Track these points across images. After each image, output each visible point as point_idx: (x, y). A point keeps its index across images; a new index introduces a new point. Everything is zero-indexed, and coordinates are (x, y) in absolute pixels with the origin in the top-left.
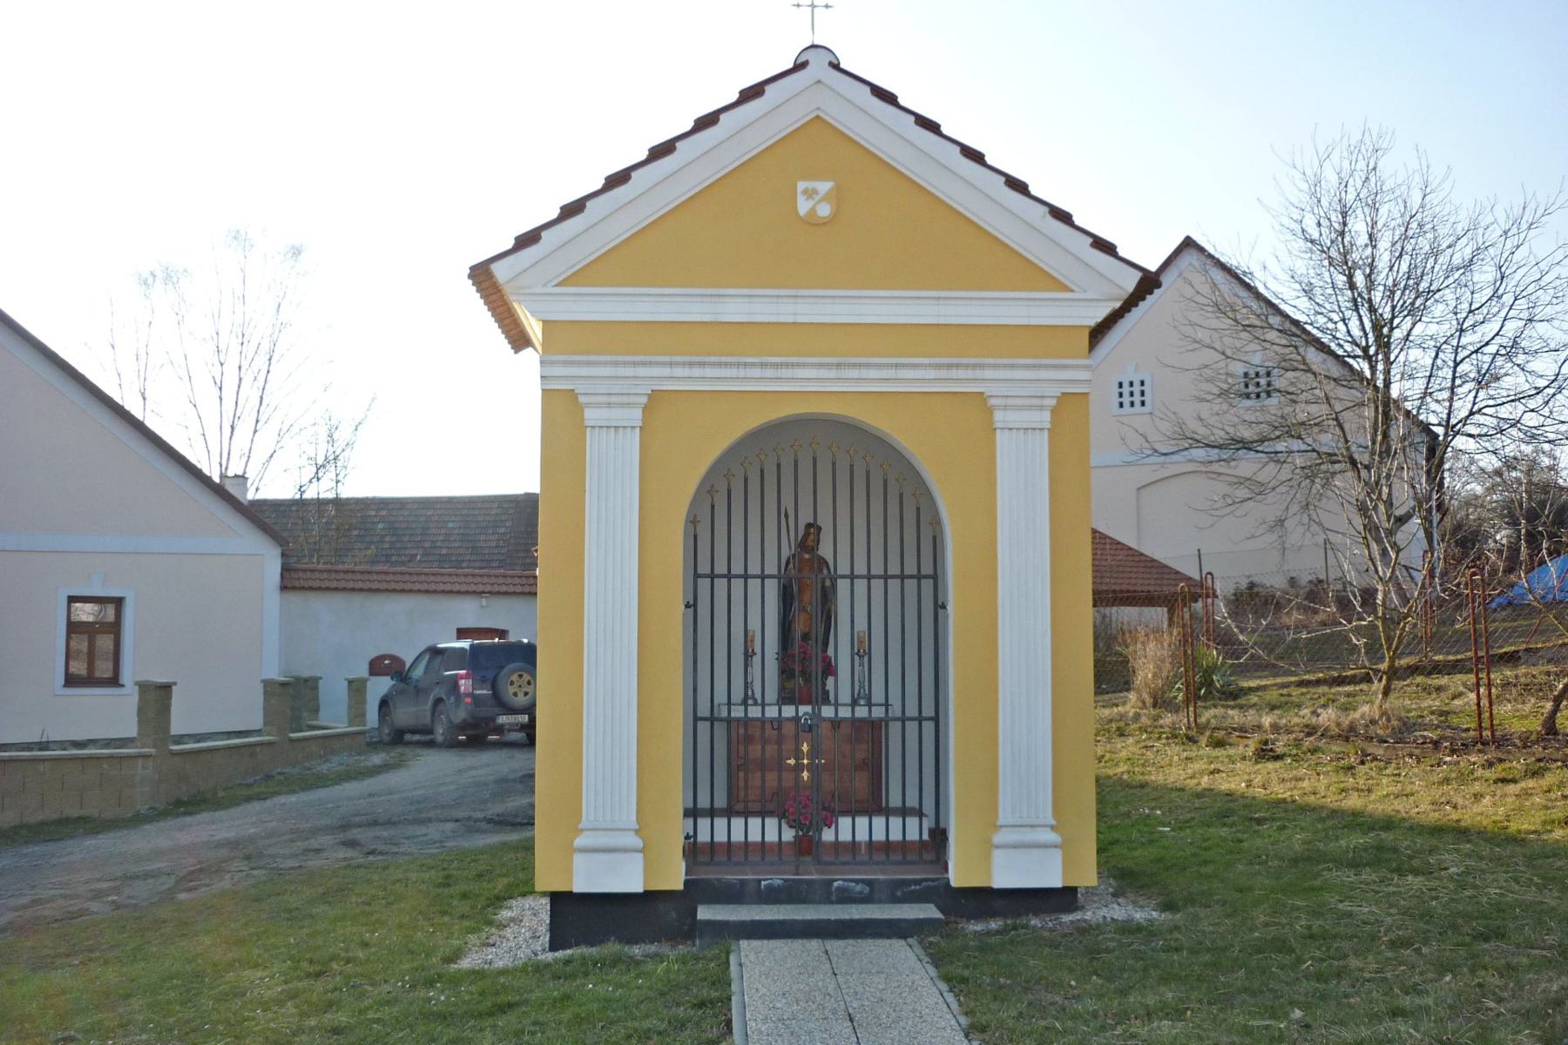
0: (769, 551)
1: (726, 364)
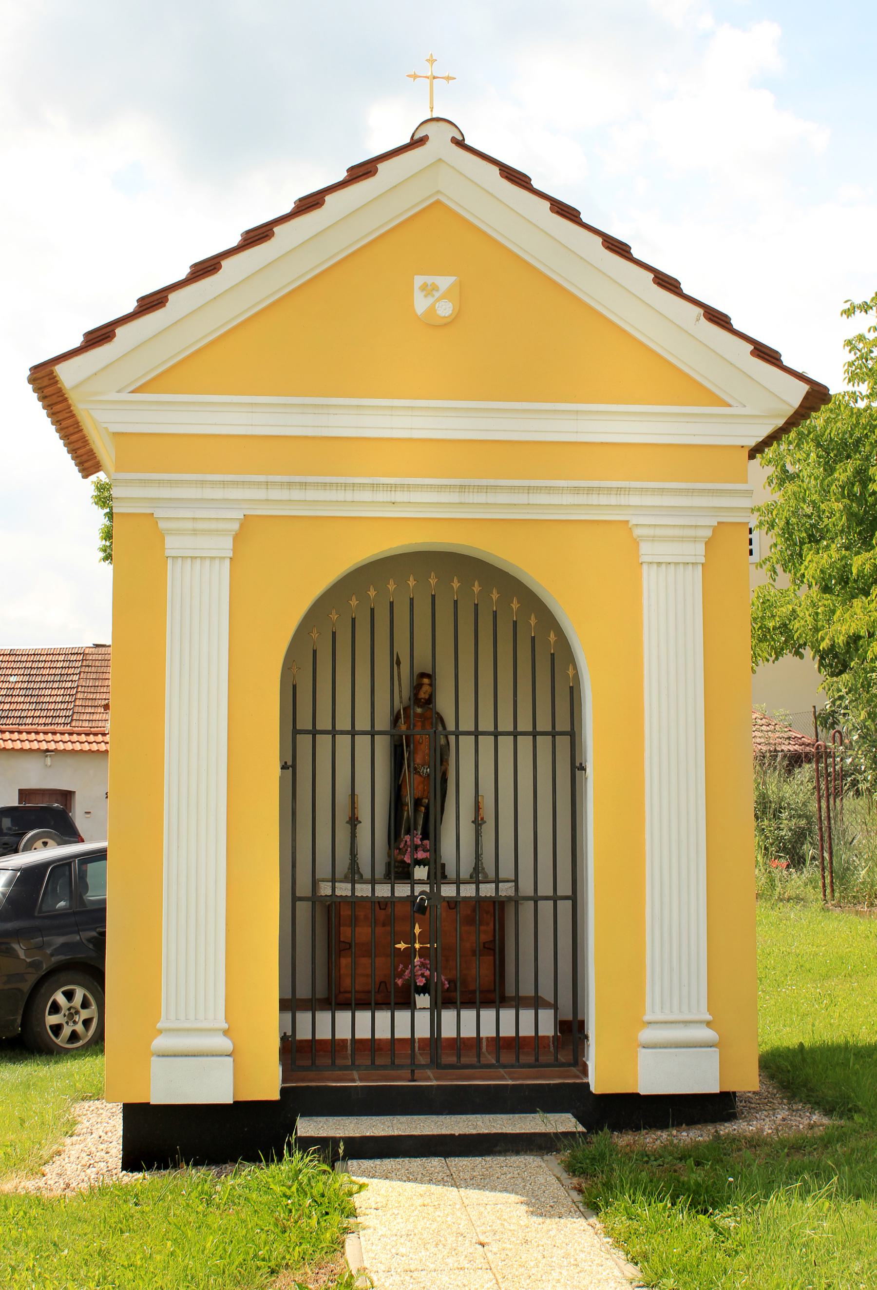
0: (366, 701)
1: (646, 490)
